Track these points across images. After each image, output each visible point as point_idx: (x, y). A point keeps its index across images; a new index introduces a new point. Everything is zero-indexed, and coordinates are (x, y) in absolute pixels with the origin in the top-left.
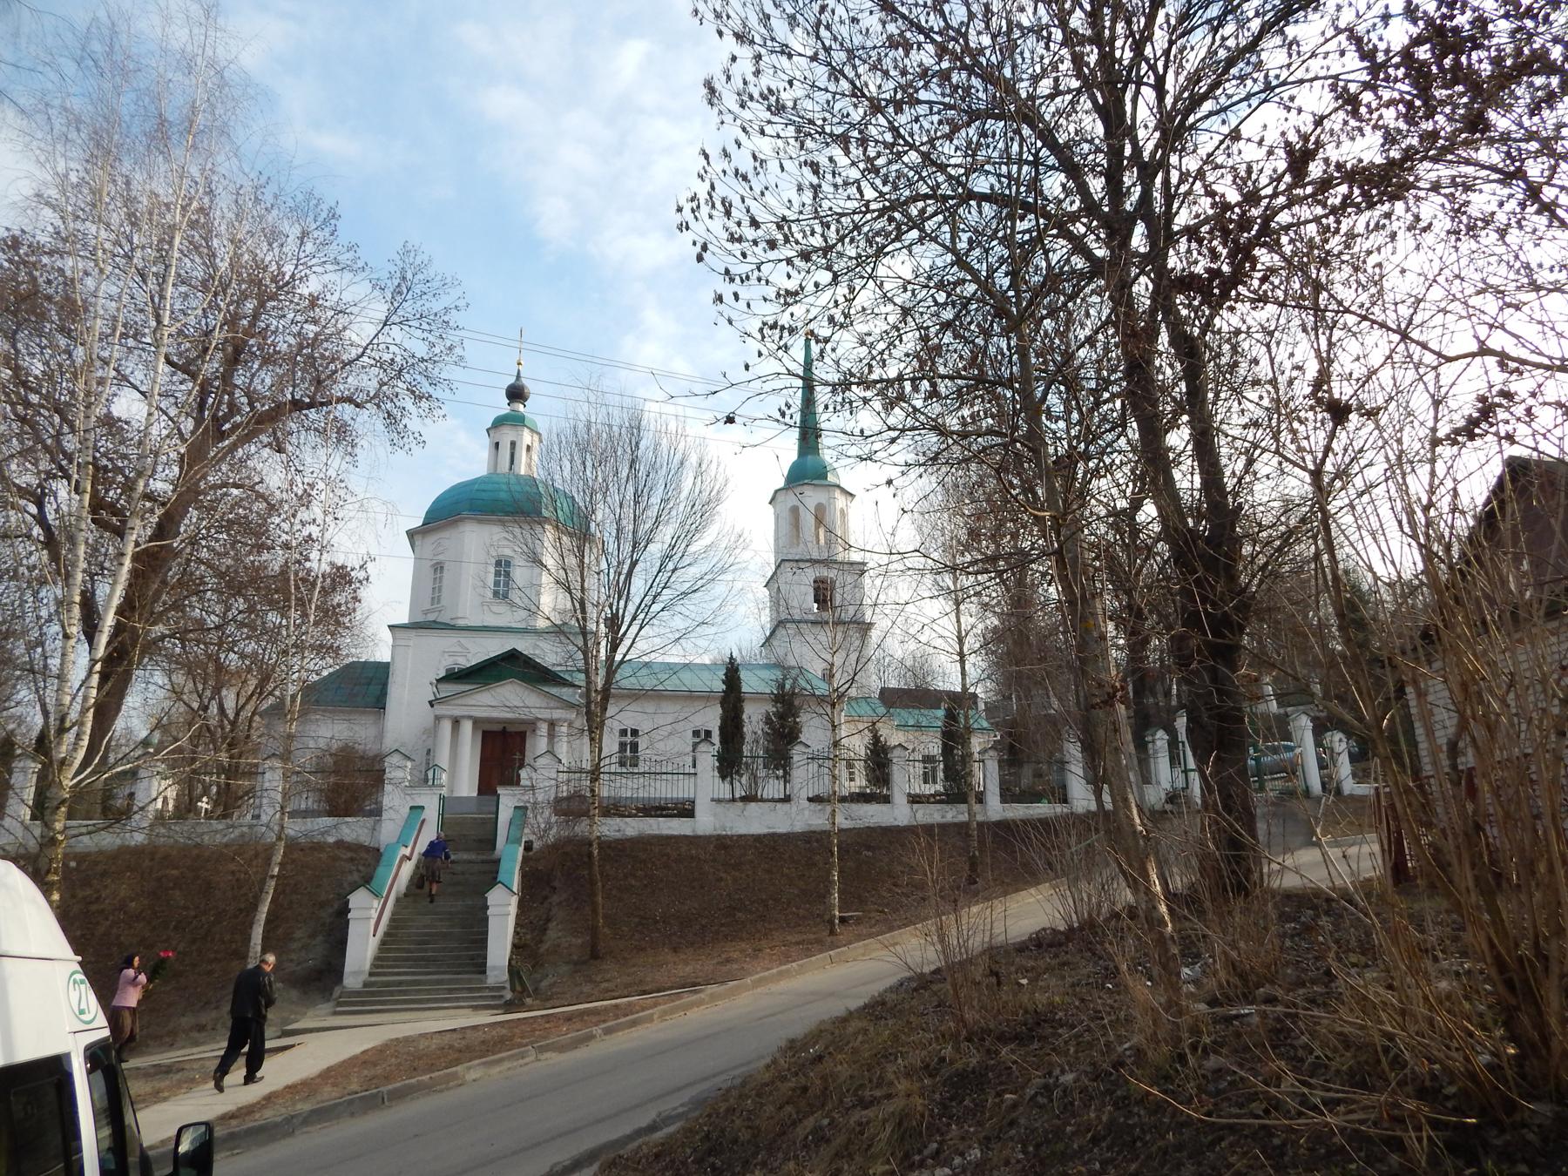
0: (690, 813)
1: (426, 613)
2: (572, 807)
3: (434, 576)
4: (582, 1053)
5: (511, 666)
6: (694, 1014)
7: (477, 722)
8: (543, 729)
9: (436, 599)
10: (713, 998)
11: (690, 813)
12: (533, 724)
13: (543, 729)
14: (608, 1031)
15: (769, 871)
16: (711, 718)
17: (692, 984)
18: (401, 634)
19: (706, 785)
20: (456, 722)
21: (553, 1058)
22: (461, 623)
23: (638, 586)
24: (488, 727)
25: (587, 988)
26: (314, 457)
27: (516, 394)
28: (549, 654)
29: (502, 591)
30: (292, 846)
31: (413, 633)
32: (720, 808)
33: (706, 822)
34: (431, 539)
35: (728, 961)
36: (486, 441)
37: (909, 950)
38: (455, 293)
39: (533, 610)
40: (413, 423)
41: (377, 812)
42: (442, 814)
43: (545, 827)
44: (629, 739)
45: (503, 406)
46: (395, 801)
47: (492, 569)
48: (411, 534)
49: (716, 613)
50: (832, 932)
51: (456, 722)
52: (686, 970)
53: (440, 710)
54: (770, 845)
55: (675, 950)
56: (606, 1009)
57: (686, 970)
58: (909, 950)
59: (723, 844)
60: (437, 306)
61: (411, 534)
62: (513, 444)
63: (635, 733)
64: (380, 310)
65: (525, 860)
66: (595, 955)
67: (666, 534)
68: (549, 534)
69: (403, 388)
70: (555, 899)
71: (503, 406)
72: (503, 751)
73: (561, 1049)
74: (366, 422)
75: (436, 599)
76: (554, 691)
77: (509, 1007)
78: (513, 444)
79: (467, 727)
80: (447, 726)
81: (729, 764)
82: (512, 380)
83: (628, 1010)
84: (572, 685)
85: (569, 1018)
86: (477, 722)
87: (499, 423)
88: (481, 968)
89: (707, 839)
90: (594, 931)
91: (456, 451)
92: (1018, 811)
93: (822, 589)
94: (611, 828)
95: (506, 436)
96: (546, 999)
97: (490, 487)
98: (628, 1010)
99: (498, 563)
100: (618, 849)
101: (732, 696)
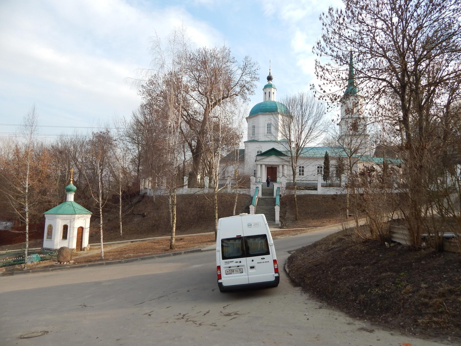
0: (316, 189)
1: (251, 138)
2: (290, 186)
3: (253, 129)
4: (296, 236)
5: (273, 152)
6: (316, 232)
7: (266, 165)
8: (281, 167)
9: (253, 134)
10: (320, 229)
11: (316, 189)
12: (278, 165)
13: (281, 167)
14: (300, 233)
15: (334, 204)
16: (322, 163)
17: (316, 226)
18: (246, 143)
19: (320, 180)
20: (261, 165)
21: (291, 236)
22: (260, 140)
23: (303, 136)
24: (268, 166)
25: (295, 226)
26: (229, 106)
27: (269, 78)
28: (280, 148)
29: (269, 132)
30: (239, 195)
31: (249, 143)
32: (323, 188)
33: (321, 191)
34: (252, 119)
35: (324, 222)
36: (262, 92)
37: (331, 228)
38: (257, 66)
39: (276, 137)
40: (248, 96)
41: (249, 188)
42: (262, 189)
43: (284, 192)
44: (301, 169)
45: (266, 82)
46: (253, 187)
47: (266, 129)
48: (247, 118)
49: (324, 130)
50: (347, 218)
51: (261, 165)
52: (314, 224)
53: (258, 163)
54: (334, 197)
55: (313, 220)
56: (300, 230)
57: (314, 224)
58: (331, 228)
59: (324, 197)
60: (253, 69)
61: (247, 118)
62: (269, 92)
63: (303, 167)
64: (240, 72)
65: (280, 199)
66: (296, 220)
67: (310, 122)
68: (280, 117)
69: (245, 89)
70: (287, 207)
71: (266, 82)
72: (272, 172)
73: (293, 235)
74: (238, 99)
75: (253, 134)
76: (282, 157)
77: (281, 228)
78: (269, 92)
79: (264, 166)
80: (259, 166)
81: (326, 177)
82: (268, 75)
83: (304, 230)
84: (287, 156)
85: (293, 231)
86: (266, 165)
87: (266, 87)
88: (274, 220)
89: (320, 195)
90: (296, 214)
91: (257, 98)
92: (272, 249)
93: (354, 125)
94: (298, 193)
95: (268, 90)
96: (288, 227)
97: (265, 105)
98: (304, 230)
99: (268, 125)
100: (300, 197)
101: (327, 158)
